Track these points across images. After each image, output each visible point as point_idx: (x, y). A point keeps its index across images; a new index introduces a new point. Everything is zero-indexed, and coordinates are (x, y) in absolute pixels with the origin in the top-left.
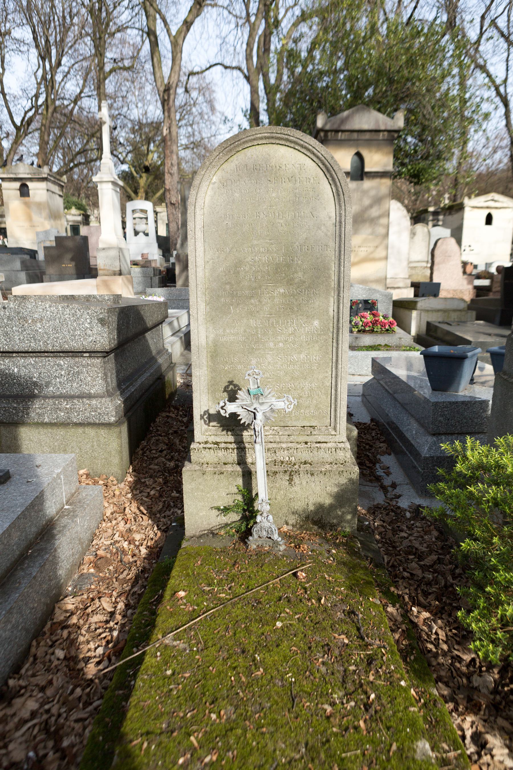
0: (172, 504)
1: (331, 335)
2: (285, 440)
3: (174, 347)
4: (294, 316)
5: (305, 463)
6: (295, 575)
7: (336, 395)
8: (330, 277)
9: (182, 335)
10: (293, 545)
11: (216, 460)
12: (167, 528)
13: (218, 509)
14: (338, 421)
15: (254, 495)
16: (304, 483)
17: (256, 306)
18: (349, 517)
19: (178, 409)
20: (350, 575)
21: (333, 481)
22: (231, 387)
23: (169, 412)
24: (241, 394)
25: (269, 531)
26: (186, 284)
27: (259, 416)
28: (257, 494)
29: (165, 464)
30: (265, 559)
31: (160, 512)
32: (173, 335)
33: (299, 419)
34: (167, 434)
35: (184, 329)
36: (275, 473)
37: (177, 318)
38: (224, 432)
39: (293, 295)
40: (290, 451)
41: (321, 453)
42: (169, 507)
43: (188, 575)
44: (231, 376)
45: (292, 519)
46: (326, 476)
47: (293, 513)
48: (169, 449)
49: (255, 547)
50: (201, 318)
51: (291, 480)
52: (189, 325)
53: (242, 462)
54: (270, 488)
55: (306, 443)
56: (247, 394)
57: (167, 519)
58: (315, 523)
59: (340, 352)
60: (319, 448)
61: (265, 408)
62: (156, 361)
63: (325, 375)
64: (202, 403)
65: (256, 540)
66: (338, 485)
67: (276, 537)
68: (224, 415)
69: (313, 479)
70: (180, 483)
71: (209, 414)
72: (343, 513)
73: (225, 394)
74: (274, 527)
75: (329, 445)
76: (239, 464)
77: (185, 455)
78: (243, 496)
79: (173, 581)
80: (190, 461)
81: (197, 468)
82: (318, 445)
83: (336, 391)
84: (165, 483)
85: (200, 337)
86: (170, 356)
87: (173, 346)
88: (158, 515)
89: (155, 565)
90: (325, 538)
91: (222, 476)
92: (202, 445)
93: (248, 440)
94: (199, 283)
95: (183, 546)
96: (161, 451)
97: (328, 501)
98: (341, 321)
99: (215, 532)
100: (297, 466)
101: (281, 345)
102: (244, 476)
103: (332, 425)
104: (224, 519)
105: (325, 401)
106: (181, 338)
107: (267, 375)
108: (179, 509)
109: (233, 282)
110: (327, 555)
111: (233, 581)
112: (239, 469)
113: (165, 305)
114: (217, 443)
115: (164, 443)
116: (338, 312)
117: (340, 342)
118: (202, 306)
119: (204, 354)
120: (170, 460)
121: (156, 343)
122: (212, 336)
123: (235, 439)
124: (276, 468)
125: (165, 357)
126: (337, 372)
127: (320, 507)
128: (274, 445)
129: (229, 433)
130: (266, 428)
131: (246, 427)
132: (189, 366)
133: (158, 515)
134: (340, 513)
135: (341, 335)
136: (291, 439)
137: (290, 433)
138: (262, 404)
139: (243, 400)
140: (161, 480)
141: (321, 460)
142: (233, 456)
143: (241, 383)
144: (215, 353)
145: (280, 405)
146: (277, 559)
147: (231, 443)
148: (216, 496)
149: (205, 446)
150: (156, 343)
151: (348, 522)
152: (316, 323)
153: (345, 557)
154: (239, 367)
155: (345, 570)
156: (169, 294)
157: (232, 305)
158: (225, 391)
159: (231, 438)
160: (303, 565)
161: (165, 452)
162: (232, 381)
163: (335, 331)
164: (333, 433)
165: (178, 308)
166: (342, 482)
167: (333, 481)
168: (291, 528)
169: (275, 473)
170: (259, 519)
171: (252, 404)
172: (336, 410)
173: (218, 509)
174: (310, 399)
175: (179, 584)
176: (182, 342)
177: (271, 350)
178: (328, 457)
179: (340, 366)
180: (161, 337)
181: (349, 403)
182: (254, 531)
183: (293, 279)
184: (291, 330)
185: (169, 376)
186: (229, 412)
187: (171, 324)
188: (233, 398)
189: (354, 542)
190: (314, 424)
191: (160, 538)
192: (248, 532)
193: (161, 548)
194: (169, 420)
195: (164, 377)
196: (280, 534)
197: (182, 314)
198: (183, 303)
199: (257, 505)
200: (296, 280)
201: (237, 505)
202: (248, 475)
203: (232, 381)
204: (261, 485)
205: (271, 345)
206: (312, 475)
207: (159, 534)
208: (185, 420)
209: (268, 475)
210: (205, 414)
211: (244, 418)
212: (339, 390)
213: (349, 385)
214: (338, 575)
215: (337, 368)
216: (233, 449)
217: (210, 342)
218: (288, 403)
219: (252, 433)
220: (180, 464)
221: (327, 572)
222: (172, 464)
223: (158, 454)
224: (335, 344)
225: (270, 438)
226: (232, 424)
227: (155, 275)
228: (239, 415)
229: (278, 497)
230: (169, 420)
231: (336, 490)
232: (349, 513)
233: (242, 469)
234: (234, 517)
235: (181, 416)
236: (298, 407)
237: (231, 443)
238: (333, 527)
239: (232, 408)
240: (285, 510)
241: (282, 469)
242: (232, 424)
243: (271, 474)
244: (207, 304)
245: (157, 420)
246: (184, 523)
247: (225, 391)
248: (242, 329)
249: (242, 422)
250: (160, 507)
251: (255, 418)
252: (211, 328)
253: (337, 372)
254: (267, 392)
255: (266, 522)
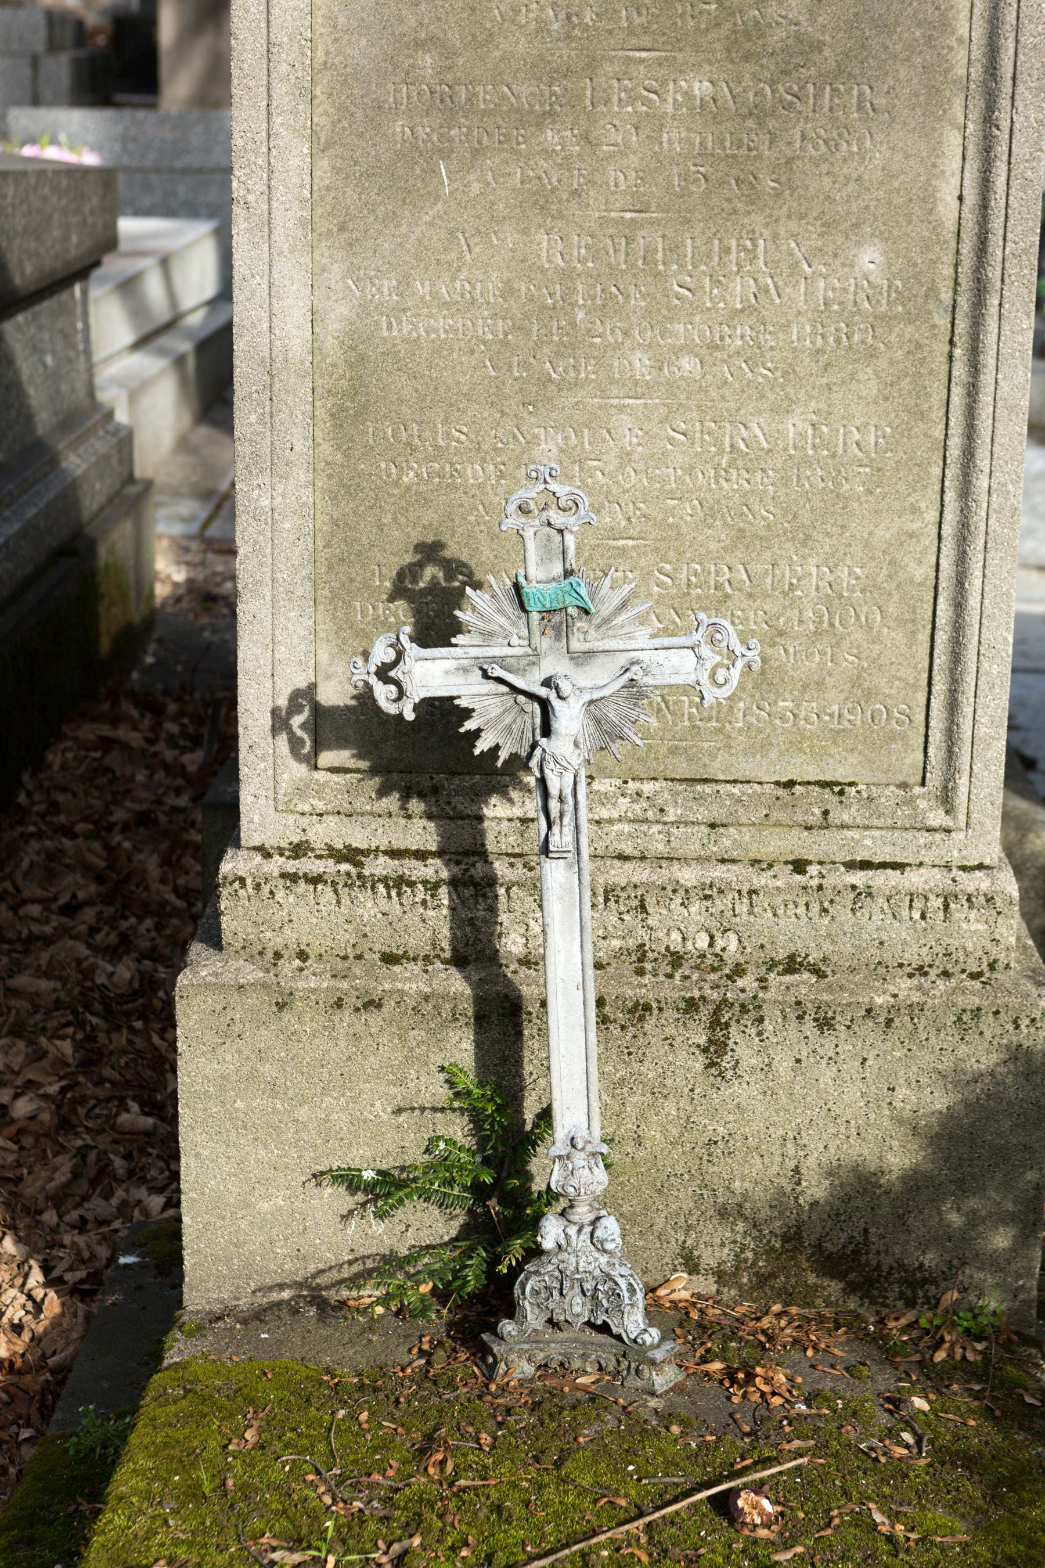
0: (119, 1164)
1: (942, 322)
2: (693, 848)
3: (145, 401)
4: (758, 219)
5: (792, 965)
6: (724, 1506)
7: (958, 626)
8: (945, 25)
9: (186, 347)
10: (717, 1366)
11: (345, 937)
12: (95, 1277)
13: (350, 1180)
14: (964, 760)
15: (529, 1117)
16: (784, 1066)
17: (567, 163)
18: (1001, 1240)
19: (158, 711)
20: (996, 1514)
21: (926, 1058)
22: (430, 572)
23: (114, 723)
24: (480, 608)
25: (604, 1294)
26: (215, 90)
27: (569, 718)
28: (546, 1115)
29: (89, 973)
30: (575, 1429)
31: (59, 1200)
32: (141, 343)
33: (765, 746)
34: (103, 828)
35: (195, 319)
36: (640, 1010)
37: (165, 263)
38: (391, 802)
39: (758, 114)
40: (720, 904)
41: (874, 919)
42: (102, 1179)
43: (194, 1493)
44: (430, 516)
45: (717, 1247)
46: (894, 1036)
47: (723, 1213)
48: (108, 899)
49: (529, 1369)
50: (288, 218)
51: (715, 1050)
52: (225, 294)
53: (474, 948)
54: (615, 1087)
55: (799, 866)
56: (510, 608)
57: (93, 1236)
58: (830, 1264)
59: (985, 412)
60: (862, 895)
61: (601, 678)
62: (54, 462)
63: (909, 529)
64: (284, 651)
65: (535, 1338)
66: (955, 1078)
67: (633, 1323)
68: (391, 709)
69: (827, 1044)
70: (163, 1064)
71: (317, 709)
72: (974, 1220)
73: (401, 607)
74: (623, 1274)
75: (914, 880)
76: (459, 961)
77: (193, 916)
78: (477, 1119)
79: (120, 1521)
80: (215, 942)
81: (252, 974)
82: (859, 878)
83: (959, 605)
84: (85, 1064)
85: (284, 321)
86: (125, 441)
87: (145, 401)
88: (50, 1217)
89: (28, 1452)
90: (880, 1341)
91: (375, 1019)
92: (277, 864)
93: (511, 841)
94: (279, 35)
95: (171, 1358)
96: (70, 910)
97: (898, 1158)
98: (996, 252)
99: (333, 1296)
100: (748, 982)
101: (688, 364)
102: (481, 1020)
103: (934, 778)
104: (380, 1234)
105: (901, 655)
106: (179, 362)
107: (614, 517)
108: (160, 1190)
109: (454, 37)
110: (884, 1419)
111: (414, 1524)
112: (457, 984)
113: (103, 193)
114: (352, 855)
115: (87, 868)
116: (984, 205)
117: (989, 360)
118: (295, 156)
119: (298, 401)
120: (113, 953)
121: (54, 376)
122: (342, 310)
123: (445, 837)
124: (643, 988)
125: (100, 445)
126: (965, 512)
127: (859, 1187)
128: (640, 873)
129: (416, 806)
130: (602, 785)
131: (501, 774)
132: (221, 503)
133: (50, 1217)
134: (955, 1219)
135: (992, 324)
136: (727, 841)
137: (717, 813)
138: (583, 658)
139: (488, 635)
140: (66, 1047)
141: (874, 953)
142: (432, 922)
143: (478, 555)
144: (356, 395)
145: (675, 666)
146: (638, 1429)
147: (421, 855)
148: (340, 1119)
149: (291, 866)
150: (54, 376)
151: (996, 1263)
152: (869, 258)
153: (975, 1430)
154: (474, 473)
155: (973, 1490)
156: (125, 139)
157: (445, 155)
158: (399, 591)
159: (422, 833)
160: (765, 1462)
161: (89, 915)
162: (438, 545)
163: (964, 303)
164: (937, 818)
165: (166, 211)
166: (972, 1066)
167: (926, 1058)
168: (707, 1285)
169: (640, 1010)
170: (551, 1232)
171: (535, 657)
172: (953, 706)
173: (350, 1180)
174: (824, 644)
175: (151, 1533)
176: (183, 382)
177: (637, 389)
178: (905, 939)
179: (982, 483)
180: (78, 346)
181: (1016, 704)
182: (529, 1288)
183: (758, 30)
184: (740, 290)
185: (115, 543)
186: (417, 693)
187: (129, 287)
188: (437, 627)
189: (1021, 1363)
190: (841, 774)
191: (56, 1323)
192: (498, 1299)
193: (62, 1372)
194: (114, 759)
195: (92, 547)
196: (654, 1312)
197: (192, 243)
198: (201, 189)
199: (545, 1171)
200: (776, 38)
201: (442, 1166)
202: (503, 1018)
203: (438, 545)
204: (569, 1070)
205: (640, 363)
206: (825, 1024)
207: (53, 1304)
208: (193, 760)
209: (603, 1020)
210: (294, 707)
211: (494, 726)
212: (973, 601)
213: (1022, 621)
214: (938, 1515)
215: (965, 492)
216: (432, 887)
217: (330, 344)
218: (712, 658)
219: (531, 806)
220: (162, 973)
221: (883, 1499)
222: (125, 972)
223: (55, 921)
224: (960, 370)
225: (621, 837)
226: (431, 761)
227: (53, 46)
228: (467, 713)
229: (653, 1133)
230: (114, 759)
231: (940, 1101)
232: (1006, 1219)
233: (477, 986)
234: (428, 1225)
235: (172, 742)
236: (762, 680)
237: (421, 855)
238: (917, 1287)
239: (431, 674)
240: (683, 1198)
241: (672, 991)
242: (431, 761)
243: (618, 1017)
244: (320, 146)
245: (55, 758)
246: (177, 1258)
247: (399, 591)
248: (494, 283)
249: (482, 746)
250: (62, 1176)
251: (547, 731)
252: (336, 271)
253: (965, 512)
254: (609, 598)
255: (583, 1246)
